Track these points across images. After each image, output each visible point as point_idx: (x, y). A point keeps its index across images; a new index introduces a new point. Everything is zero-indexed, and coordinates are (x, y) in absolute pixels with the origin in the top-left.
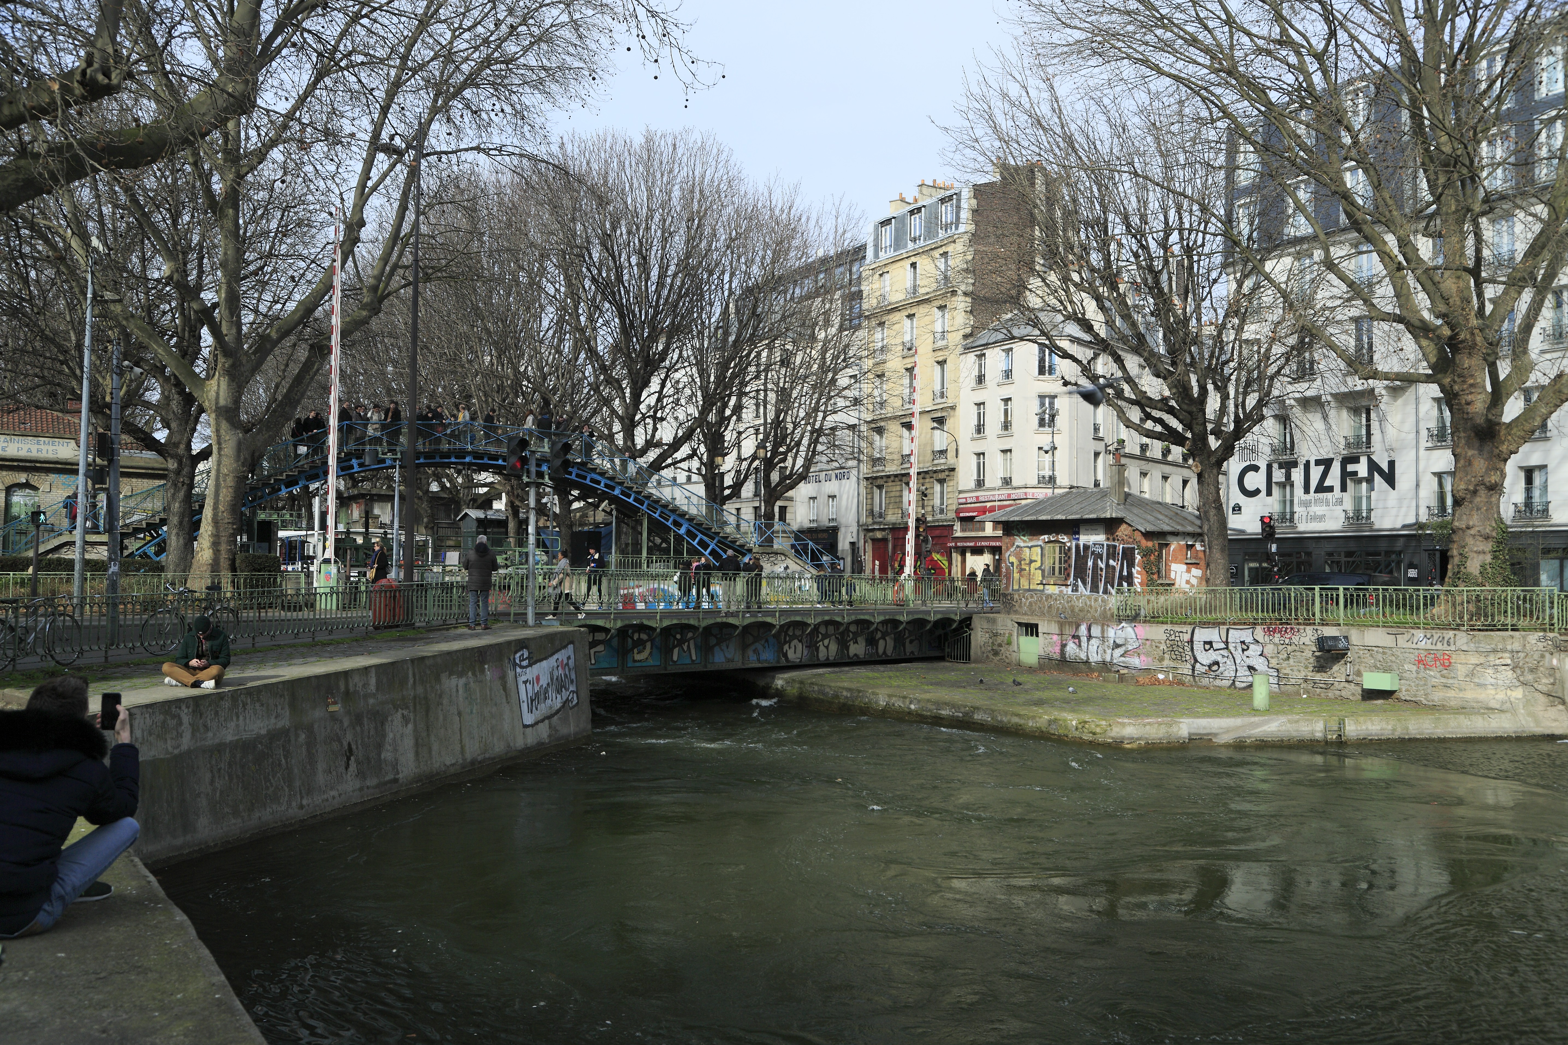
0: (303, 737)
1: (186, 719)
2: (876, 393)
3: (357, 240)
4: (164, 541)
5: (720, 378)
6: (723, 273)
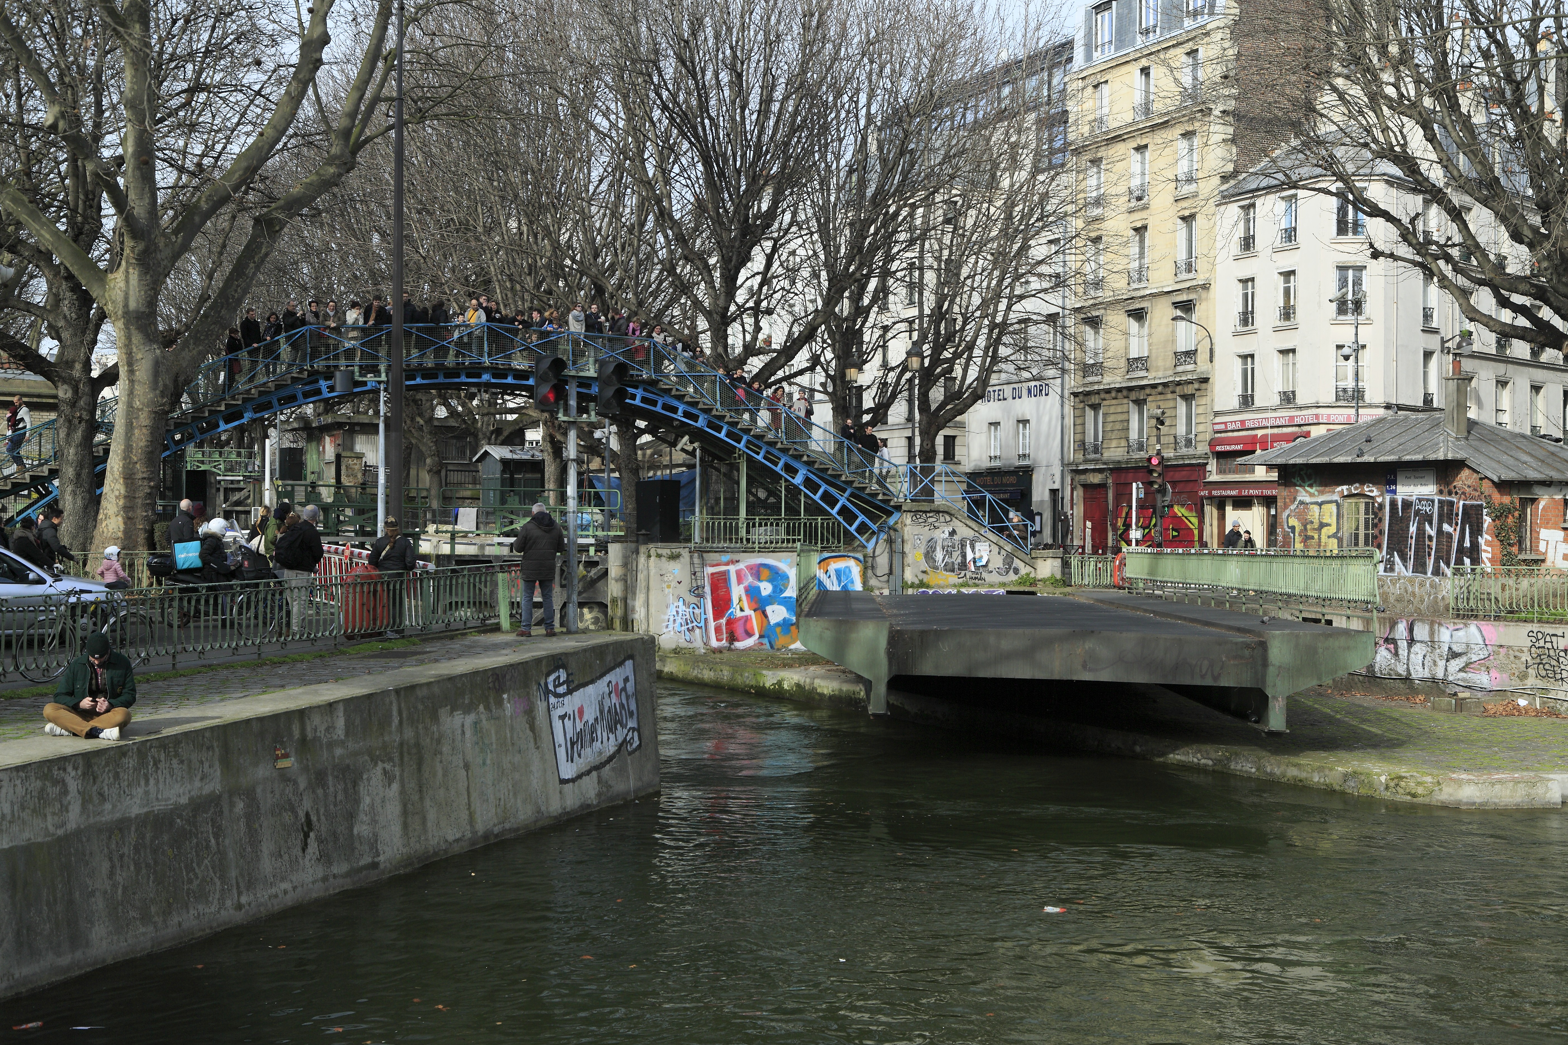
0: (240, 806)
1: (73, 786)
2: (1087, 268)
3: (318, 63)
4: (56, 501)
5: (856, 247)
6: (858, 91)
